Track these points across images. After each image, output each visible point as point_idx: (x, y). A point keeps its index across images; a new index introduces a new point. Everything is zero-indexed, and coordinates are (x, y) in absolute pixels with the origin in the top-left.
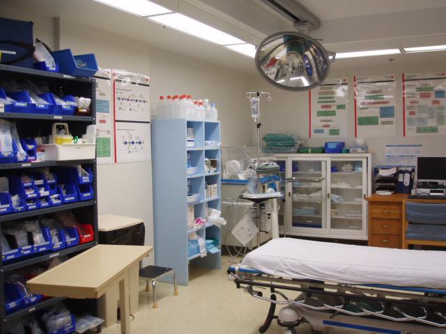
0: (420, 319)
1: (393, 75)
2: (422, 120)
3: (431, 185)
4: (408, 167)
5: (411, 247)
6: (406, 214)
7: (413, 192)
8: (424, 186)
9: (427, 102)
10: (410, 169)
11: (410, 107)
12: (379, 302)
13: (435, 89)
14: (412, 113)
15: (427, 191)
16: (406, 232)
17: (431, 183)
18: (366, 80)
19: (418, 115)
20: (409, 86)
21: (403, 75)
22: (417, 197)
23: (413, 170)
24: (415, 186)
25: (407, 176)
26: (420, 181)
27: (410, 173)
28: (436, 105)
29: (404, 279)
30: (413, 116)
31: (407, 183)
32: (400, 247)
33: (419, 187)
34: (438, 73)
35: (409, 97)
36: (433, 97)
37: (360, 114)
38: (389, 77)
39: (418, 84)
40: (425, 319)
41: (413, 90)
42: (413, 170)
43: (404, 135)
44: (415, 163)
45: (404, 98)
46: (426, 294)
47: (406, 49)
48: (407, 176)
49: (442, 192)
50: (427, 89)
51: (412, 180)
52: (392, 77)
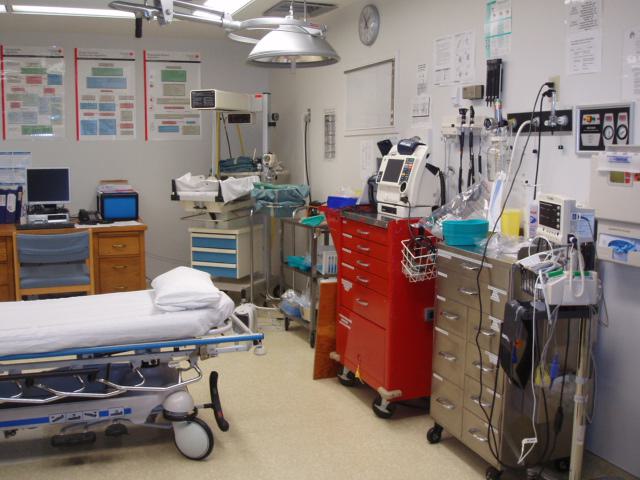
0: (137, 387)
1: (199, 54)
2: (31, 115)
3: (47, 209)
4: (11, 184)
5: (25, 298)
6: (19, 252)
7: (23, 221)
8: (38, 210)
9: (37, 90)
10: (15, 188)
11: (11, 97)
12: (13, 381)
13: (48, 72)
14: (15, 105)
15: (44, 217)
16: (21, 279)
17: (46, 206)
18: (20, 53)
19: (24, 109)
20: (9, 64)
21: (76, 50)
22: (29, 227)
23: (20, 189)
24: (23, 212)
25: (12, 198)
26: (32, 203)
27: (16, 193)
28: (49, 95)
29: (52, 340)
30: (16, 110)
31: (12, 208)
32: (15, 300)
33: (29, 213)
34: (190, 54)
35: (9, 81)
36: (45, 83)
37: (625, 114)
38: (126, 54)
39: (23, 63)
40: (143, 386)
41: (16, 71)
42: (20, 189)
43: (4, 137)
44: (23, 180)
45: (2, 81)
46: (80, 357)
47: (15, 7)
48: (12, 198)
49: (64, 217)
50: (36, 71)
51: (18, 204)
52: (131, 54)
